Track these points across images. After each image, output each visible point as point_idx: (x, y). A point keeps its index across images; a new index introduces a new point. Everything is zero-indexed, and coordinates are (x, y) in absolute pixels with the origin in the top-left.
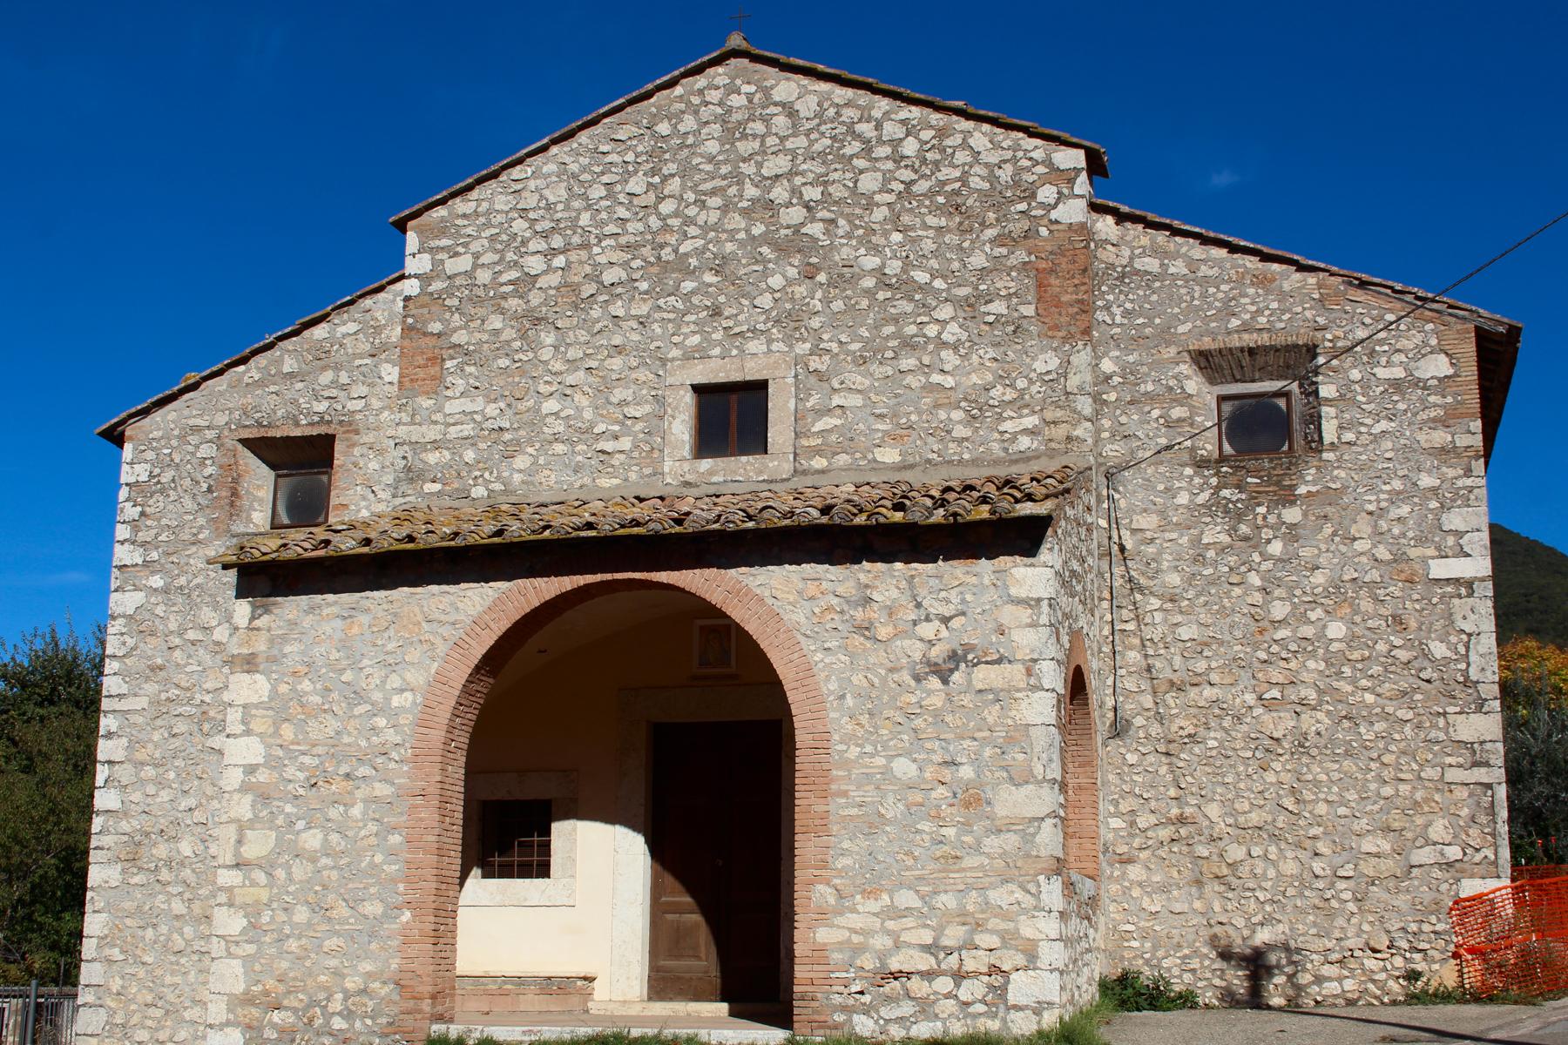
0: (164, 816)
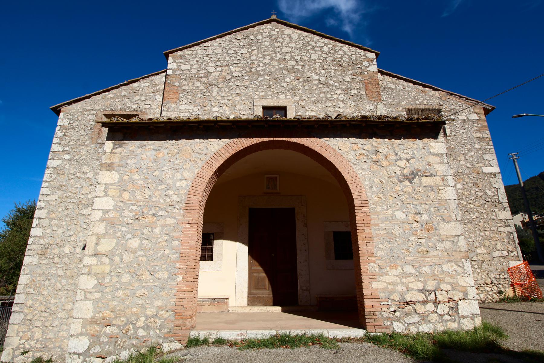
0: (59, 238)
